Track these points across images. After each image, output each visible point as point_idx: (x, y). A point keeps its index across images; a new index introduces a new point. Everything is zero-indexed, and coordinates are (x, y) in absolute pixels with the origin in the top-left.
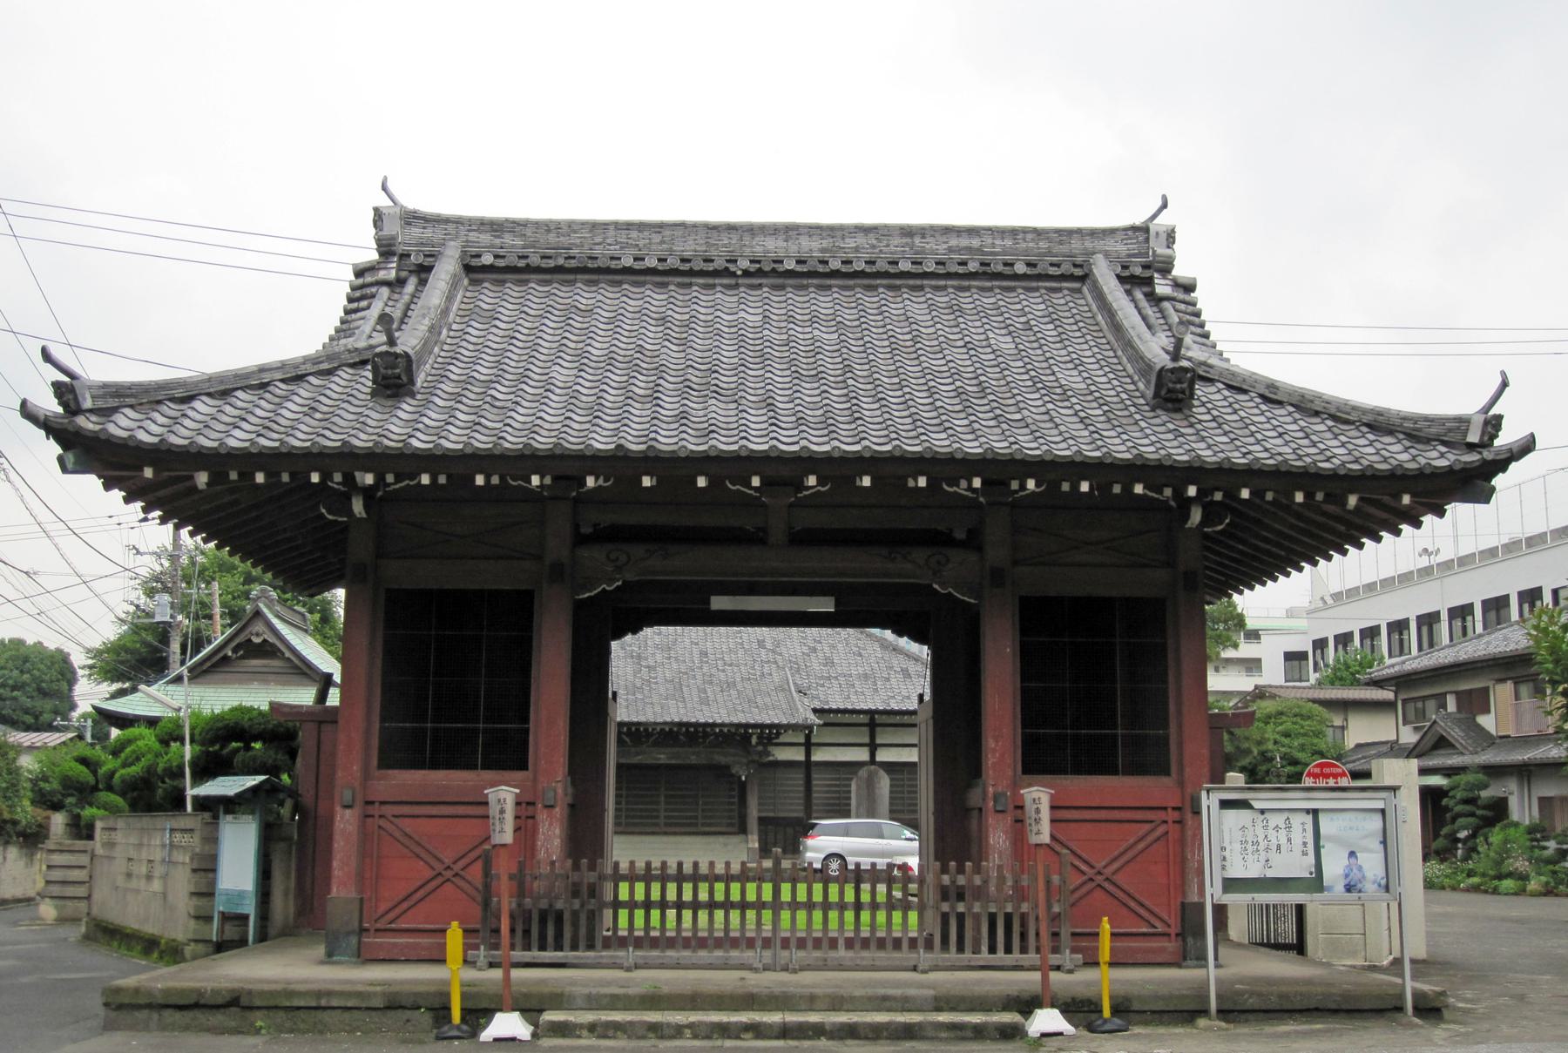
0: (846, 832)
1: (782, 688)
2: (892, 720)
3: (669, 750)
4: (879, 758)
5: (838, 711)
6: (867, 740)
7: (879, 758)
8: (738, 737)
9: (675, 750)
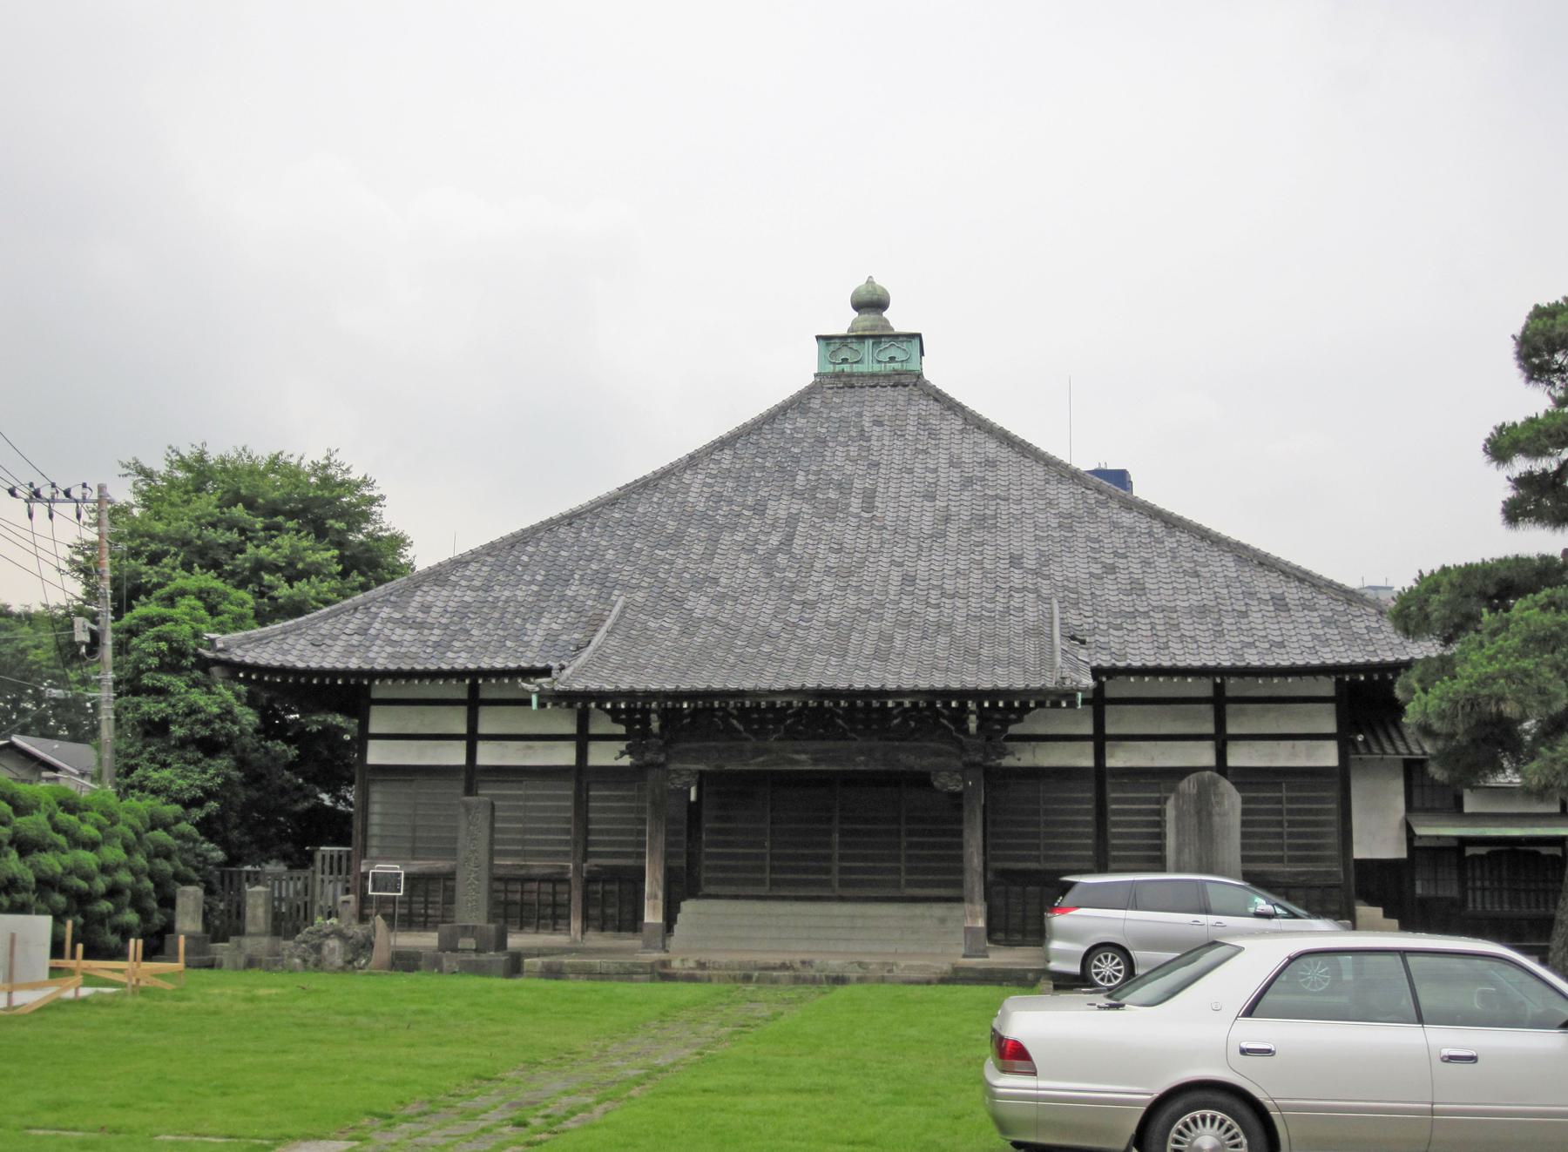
0: (1132, 899)
1: (1038, 632)
2: (1261, 687)
3: (817, 745)
4: (1233, 761)
5: (1143, 671)
6: (1209, 728)
7: (1233, 761)
8: (935, 713)
9: (830, 744)
